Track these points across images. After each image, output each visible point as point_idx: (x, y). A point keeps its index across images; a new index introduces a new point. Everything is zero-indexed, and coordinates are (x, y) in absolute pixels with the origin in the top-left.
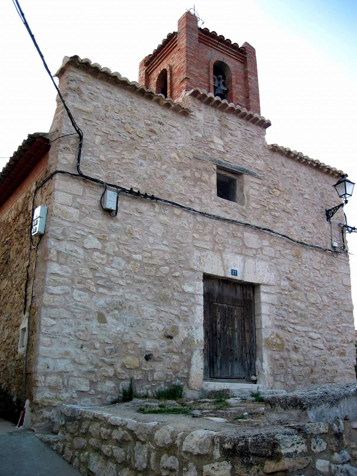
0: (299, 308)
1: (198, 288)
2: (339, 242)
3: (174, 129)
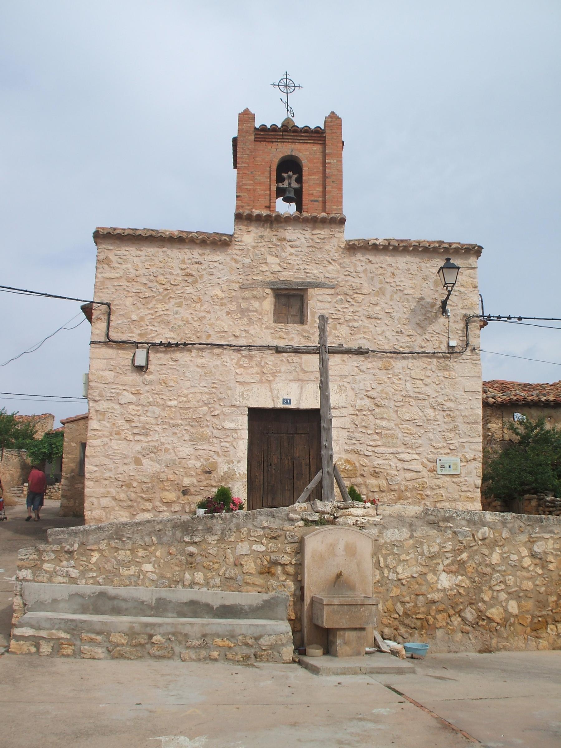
0: (383, 428)
1: (242, 422)
2: (461, 338)
3: (215, 264)
